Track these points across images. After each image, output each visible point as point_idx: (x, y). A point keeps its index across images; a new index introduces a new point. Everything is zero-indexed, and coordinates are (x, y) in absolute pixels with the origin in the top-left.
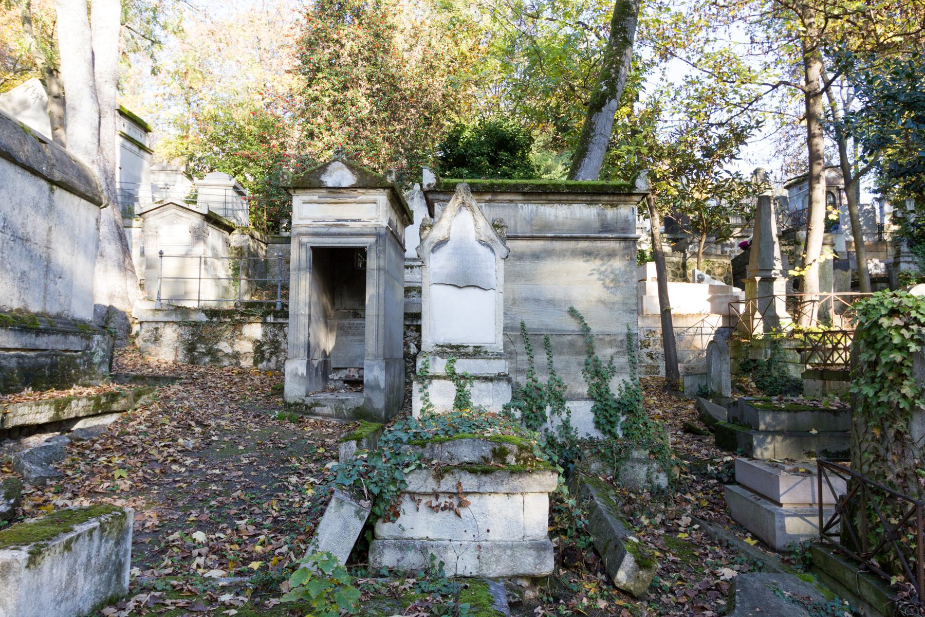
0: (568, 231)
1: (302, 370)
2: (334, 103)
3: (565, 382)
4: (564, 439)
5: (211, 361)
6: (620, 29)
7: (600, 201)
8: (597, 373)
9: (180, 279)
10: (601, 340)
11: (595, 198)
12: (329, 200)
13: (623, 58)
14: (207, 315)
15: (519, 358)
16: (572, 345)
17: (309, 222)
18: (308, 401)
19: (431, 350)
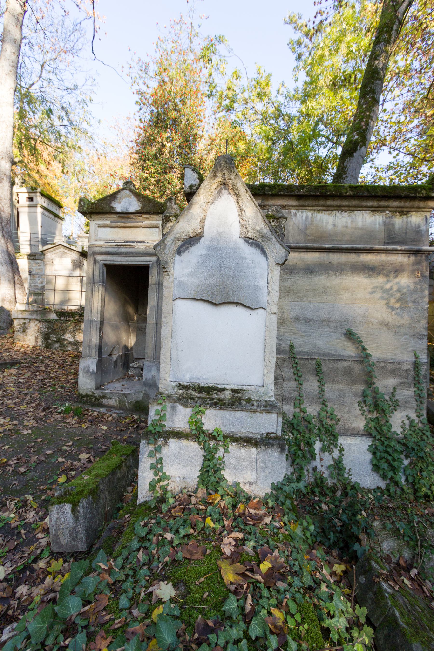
0: (348, 242)
1: (93, 367)
2: (158, 181)
3: (338, 414)
4: (335, 481)
5: (59, 346)
6: (370, 91)
7: (387, 207)
8: (376, 406)
9: (66, 291)
10: (382, 368)
11: (383, 203)
12: (119, 224)
13: (372, 114)
14: (57, 315)
15: (286, 384)
16: (347, 372)
17: (102, 243)
18: (97, 393)
19: (171, 391)
